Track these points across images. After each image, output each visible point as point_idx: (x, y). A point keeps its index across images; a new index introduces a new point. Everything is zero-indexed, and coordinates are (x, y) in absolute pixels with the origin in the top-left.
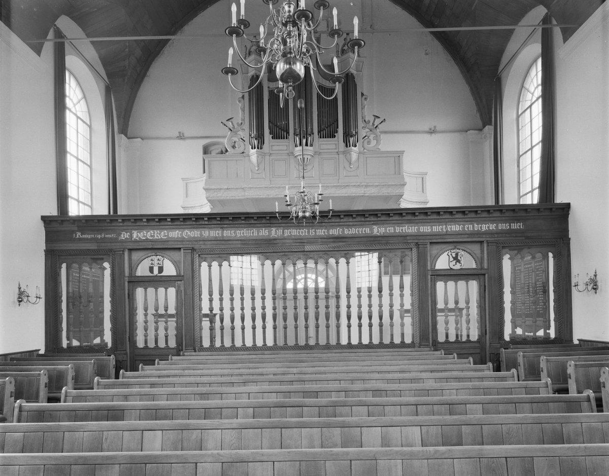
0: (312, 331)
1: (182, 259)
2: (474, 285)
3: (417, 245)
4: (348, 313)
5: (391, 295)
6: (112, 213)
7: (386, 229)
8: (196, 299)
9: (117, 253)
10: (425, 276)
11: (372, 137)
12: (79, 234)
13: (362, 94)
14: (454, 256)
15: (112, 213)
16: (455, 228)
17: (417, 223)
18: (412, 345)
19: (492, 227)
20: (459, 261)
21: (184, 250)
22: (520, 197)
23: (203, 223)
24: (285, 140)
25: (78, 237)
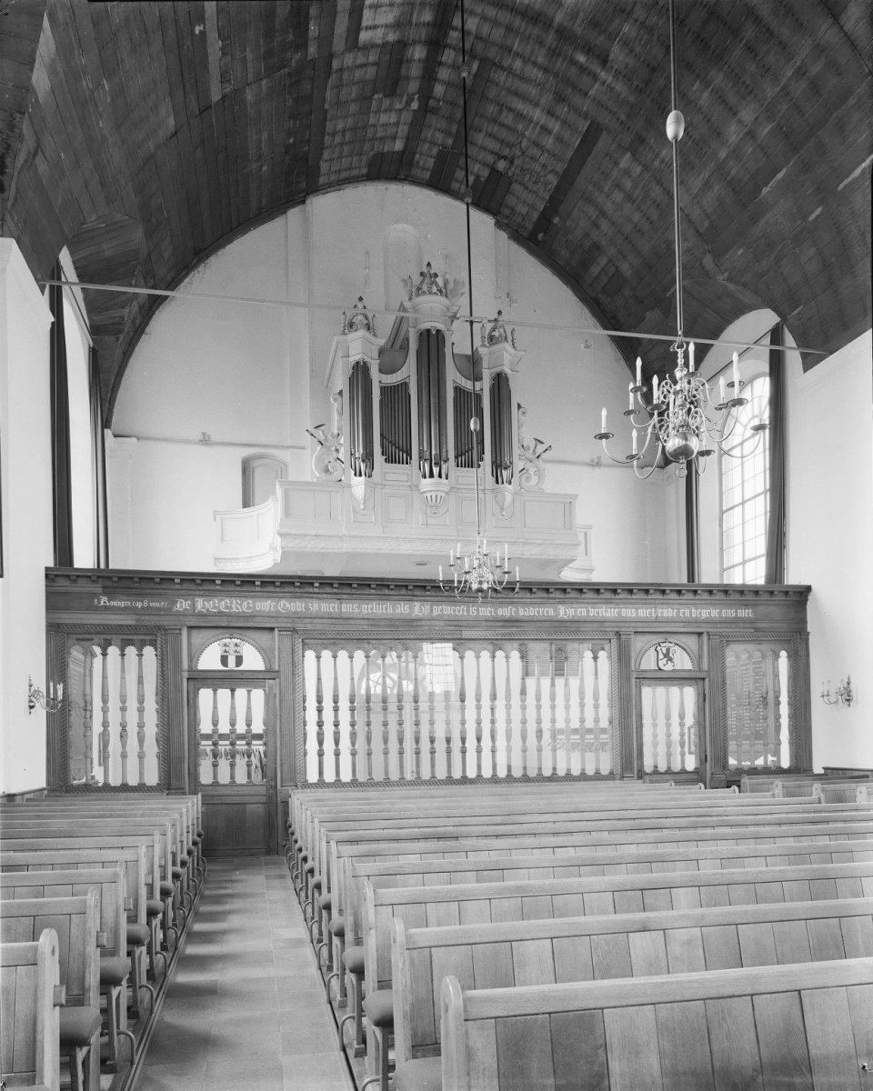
0: (378, 758)
1: (277, 644)
2: (690, 693)
3: (618, 634)
4: (522, 731)
5: (479, 708)
6: (102, 566)
7: (575, 612)
8: (299, 708)
9: (170, 632)
10: (629, 679)
11: (532, 470)
12: (104, 600)
13: (519, 406)
14: (665, 652)
15: (102, 566)
16: (667, 612)
17: (617, 604)
18: (611, 776)
19: (714, 613)
20: (671, 659)
21: (280, 631)
22: (723, 570)
23: (311, 590)
24: (405, 465)
25: (102, 604)
